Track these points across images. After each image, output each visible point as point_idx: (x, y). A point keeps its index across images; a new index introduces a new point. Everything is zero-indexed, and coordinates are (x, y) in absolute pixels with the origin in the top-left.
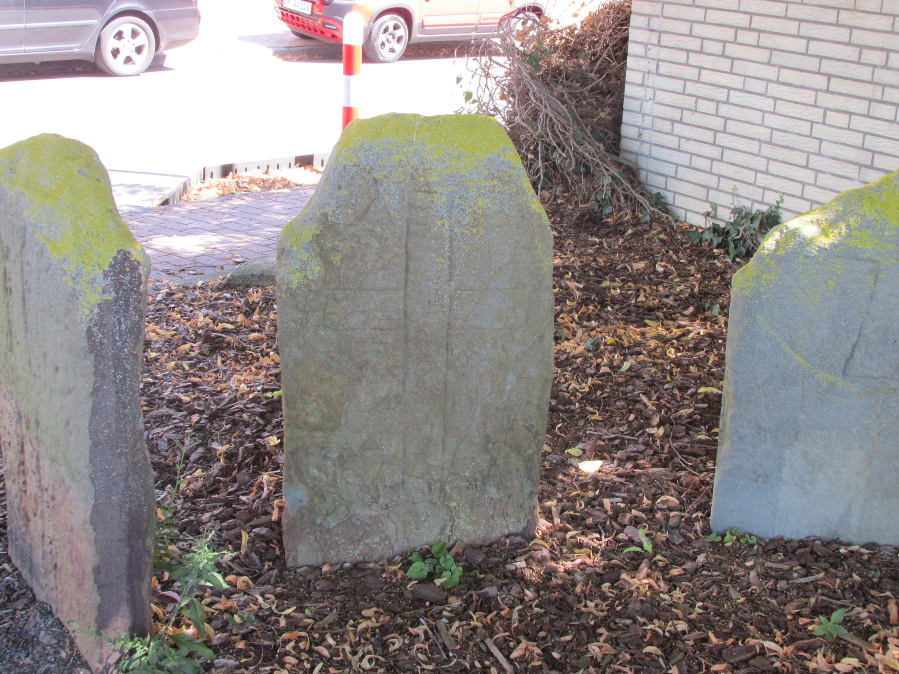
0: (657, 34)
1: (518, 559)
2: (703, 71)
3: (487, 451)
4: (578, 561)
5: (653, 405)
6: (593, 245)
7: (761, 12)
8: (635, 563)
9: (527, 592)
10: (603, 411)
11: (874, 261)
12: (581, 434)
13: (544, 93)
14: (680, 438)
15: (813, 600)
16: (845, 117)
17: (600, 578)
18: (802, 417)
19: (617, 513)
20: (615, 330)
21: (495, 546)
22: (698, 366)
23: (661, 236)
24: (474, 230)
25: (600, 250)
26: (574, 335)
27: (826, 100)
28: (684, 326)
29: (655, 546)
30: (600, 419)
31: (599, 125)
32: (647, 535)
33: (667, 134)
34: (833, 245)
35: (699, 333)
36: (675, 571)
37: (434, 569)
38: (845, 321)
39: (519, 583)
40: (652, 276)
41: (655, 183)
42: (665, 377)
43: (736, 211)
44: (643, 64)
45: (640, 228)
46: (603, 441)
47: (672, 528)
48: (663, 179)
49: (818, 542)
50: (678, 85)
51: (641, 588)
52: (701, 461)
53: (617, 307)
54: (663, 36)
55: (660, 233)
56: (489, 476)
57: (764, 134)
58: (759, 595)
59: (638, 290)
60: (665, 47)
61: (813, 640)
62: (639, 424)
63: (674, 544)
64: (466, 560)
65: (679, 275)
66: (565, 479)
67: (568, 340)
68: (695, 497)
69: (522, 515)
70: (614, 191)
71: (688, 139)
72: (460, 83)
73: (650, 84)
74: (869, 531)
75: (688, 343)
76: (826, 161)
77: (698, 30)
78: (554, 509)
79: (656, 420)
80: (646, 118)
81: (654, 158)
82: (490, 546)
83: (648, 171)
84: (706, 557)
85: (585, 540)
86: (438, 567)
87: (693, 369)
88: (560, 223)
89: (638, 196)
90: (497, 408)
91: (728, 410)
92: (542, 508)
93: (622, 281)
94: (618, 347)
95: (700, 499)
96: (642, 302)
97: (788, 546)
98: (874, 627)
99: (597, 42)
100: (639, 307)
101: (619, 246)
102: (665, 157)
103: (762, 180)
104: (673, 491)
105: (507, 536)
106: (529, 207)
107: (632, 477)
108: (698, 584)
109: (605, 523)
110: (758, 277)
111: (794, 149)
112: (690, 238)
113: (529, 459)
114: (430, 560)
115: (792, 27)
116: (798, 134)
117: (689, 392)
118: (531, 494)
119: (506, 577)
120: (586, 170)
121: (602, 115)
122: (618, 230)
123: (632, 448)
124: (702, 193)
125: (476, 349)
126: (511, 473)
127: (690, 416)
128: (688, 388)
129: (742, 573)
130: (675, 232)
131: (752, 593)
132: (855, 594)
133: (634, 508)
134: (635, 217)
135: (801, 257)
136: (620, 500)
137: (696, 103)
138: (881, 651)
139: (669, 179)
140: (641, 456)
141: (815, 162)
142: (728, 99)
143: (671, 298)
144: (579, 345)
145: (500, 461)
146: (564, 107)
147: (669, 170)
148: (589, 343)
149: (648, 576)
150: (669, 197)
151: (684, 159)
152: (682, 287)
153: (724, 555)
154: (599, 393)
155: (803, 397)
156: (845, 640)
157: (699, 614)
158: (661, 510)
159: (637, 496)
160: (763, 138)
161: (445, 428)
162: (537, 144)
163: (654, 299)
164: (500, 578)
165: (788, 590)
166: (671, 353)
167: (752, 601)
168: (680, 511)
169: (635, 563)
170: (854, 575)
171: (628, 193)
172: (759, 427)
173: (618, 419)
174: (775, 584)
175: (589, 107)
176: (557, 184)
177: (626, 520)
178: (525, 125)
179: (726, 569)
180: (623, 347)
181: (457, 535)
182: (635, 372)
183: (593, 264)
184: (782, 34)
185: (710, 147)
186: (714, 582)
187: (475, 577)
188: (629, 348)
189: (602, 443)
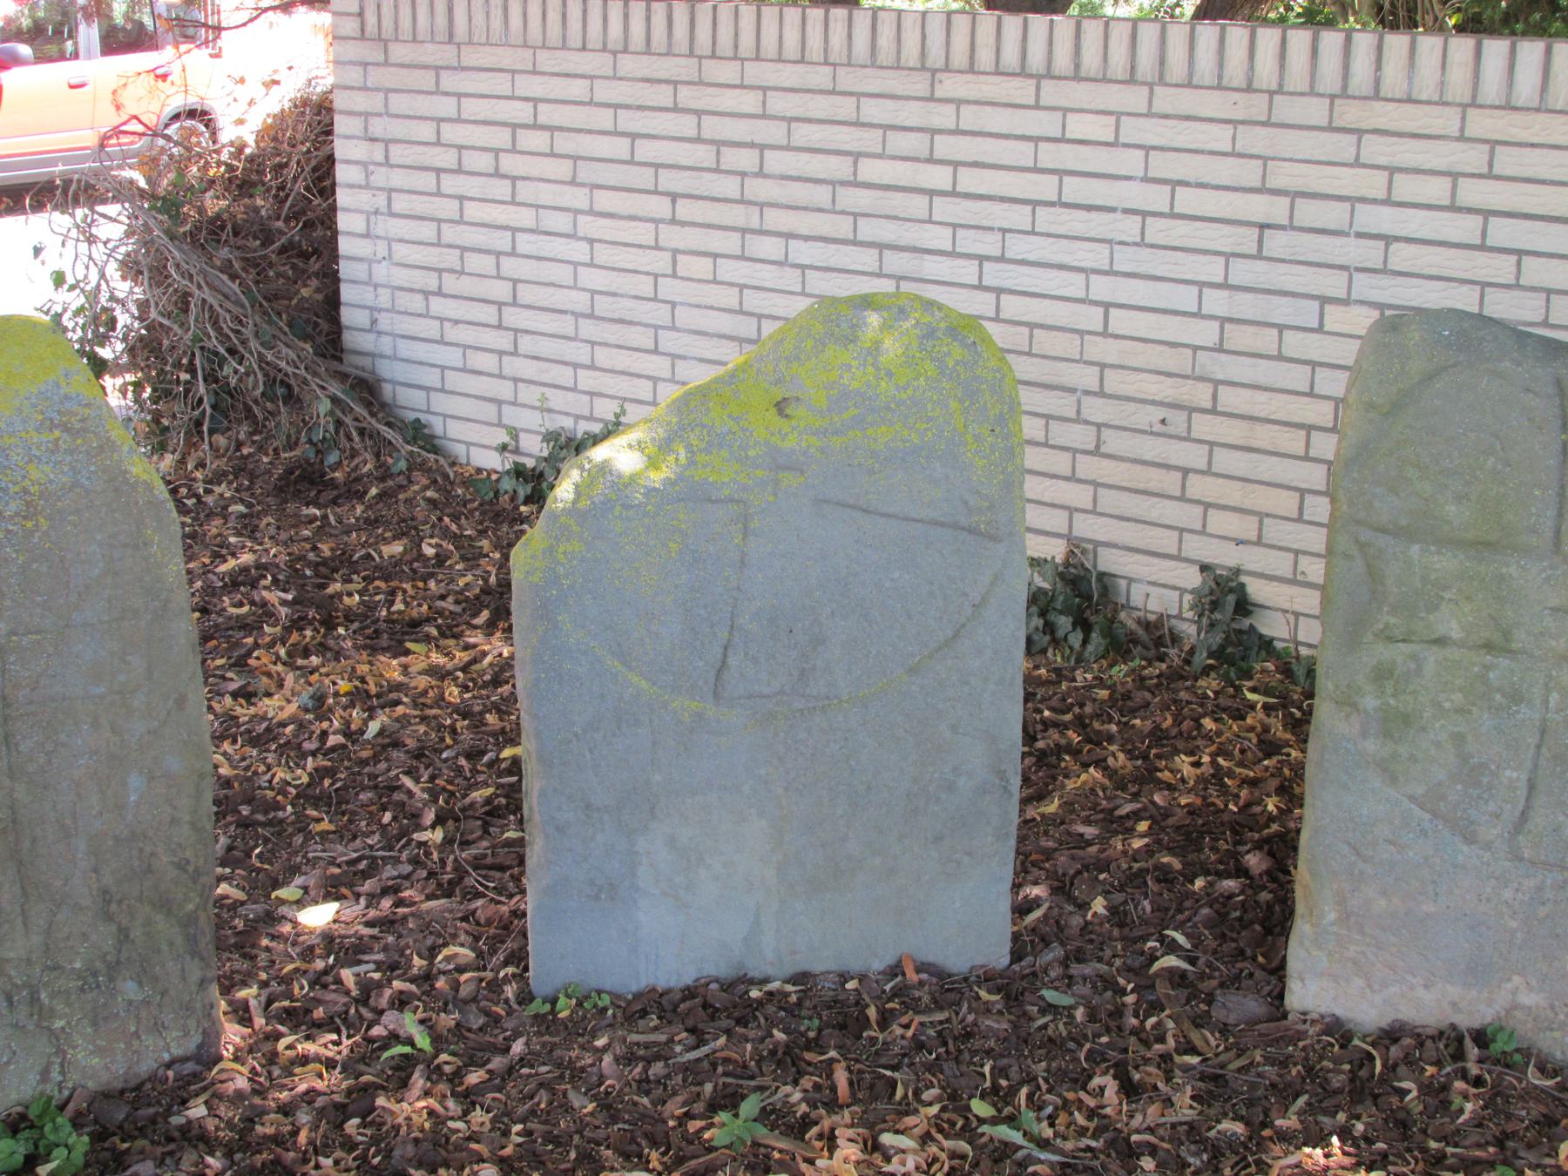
0: (382, 145)
1: (191, 1103)
2: (467, 204)
3: (109, 918)
4: (303, 1087)
5: (423, 790)
6: (311, 522)
7: (551, 96)
8: (403, 1075)
9: (210, 1160)
10: (336, 813)
11: (738, 502)
12: (299, 859)
13: (195, 263)
14: (474, 842)
15: (708, 1087)
16: (707, 262)
17: (341, 1112)
18: (658, 778)
19: (367, 989)
20: (354, 669)
21: (149, 1086)
22: (499, 711)
23: (429, 494)
24: (29, 524)
25: (323, 529)
26: (281, 686)
27: (674, 237)
28: (475, 646)
29: (438, 1040)
30: (332, 828)
31: (302, 310)
32: (422, 1022)
33: (420, 315)
34: (668, 482)
35: (500, 655)
36: (474, 1078)
37: (36, 1147)
38: (705, 607)
39: (196, 1147)
40: (416, 565)
41: (410, 402)
42: (442, 740)
43: (551, 437)
44: (364, 199)
45: (391, 483)
46: (339, 866)
47: (466, 1002)
48: (423, 394)
49: (714, 986)
50: (427, 231)
51: (414, 1116)
52: (512, 876)
53: (356, 625)
54: (392, 148)
55: (426, 488)
56: (118, 962)
57: (580, 301)
58: (620, 1093)
59: (393, 593)
60: (399, 166)
61: (713, 1155)
62: (401, 827)
63: (469, 1030)
64: (96, 1122)
65: (463, 558)
66: (274, 944)
67: (269, 695)
68: (503, 942)
69: (192, 1023)
70: (339, 423)
71: (456, 322)
72: (41, 257)
73: (381, 233)
74: (794, 953)
75: (483, 672)
76: (686, 339)
77: (450, 133)
78: (253, 1003)
79: (429, 817)
80: (380, 291)
81: (403, 360)
82: (138, 1087)
83: (395, 383)
84: (527, 1044)
85: (311, 1048)
86: (42, 1143)
87: (490, 718)
88: (249, 488)
89: (383, 429)
90: (116, 839)
91: (534, 785)
92: (230, 1003)
93: (364, 579)
94: (359, 696)
95: (510, 944)
96: (400, 612)
97: (664, 1001)
98: (813, 1115)
99: (286, 165)
100: (393, 622)
101: (357, 519)
102: (422, 357)
103: (587, 380)
104: (463, 937)
105: (169, 1066)
106: (126, 472)
107: (392, 922)
108: (514, 1092)
109: (347, 1012)
110: (551, 550)
111: (631, 323)
112: (477, 491)
113: (189, 922)
114: (26, 1134)
115: (604, 119)
116: (636, 297)
117: (486, 759)
118: (203, 983)
119: (170, 1139)
120: (287, 392)
121: (305, 292)
122: (353, 491)
123: (389, 871)
124: (489, 411)
125: (63, 737)
126: (159, 951)
127: (489, 801)
128: (484, 753)
129: (590, 1061)
130: (452, 483)
131: (607, 1093)
132: (779, 1063)
133: (398, 977)
134: (381, 465)
135: (618, 508)
136: (372, 966)
137: (462, 258)
138: (826, 1153)
139: (432, 394)
140: (407, 883)
141: (669, 341)
142: (514, 248)
143: (450, 599)
144: (289, 701)
145: (137, 933)
146: (235, 286)
147: (431, 378)
148: (305, 697)
149: (427, 1093)
150: (437, 426)
151: (452, 357)
152: (469, 578)
153: (557, 1033)
154: (327, 782)
155: (654, 744)
156: (766, 1146)
157: (519, 1145)
158: (444, 973)
159: (402, 954)
160: (579, 308)
161: (23, 888)
162: (193, 355)
163: (420, 605)
164: (159, 1143)
165: (668, 1076)
166: (453, 693)
167: (608, 1107)
168: (478, 969)
169: (403, 1075)
170: (775, 1032)
171: (364, 425)
172: (588, 806)
173: (364, 823)
174: (646, 1070)
175: (281, 281)
176: (239, 422)
177: (384, 1002)
178: (165, 322)
179: (562, 1058)
180: (369, 696)
181: (74, 1078)
182: (389, 736)
183: (311, 556)
184: (590, 132)
185: (494, 333)
186: (541, 1085)
187: (113, 1149)
188: (378, 696)
189: (337, 871)
